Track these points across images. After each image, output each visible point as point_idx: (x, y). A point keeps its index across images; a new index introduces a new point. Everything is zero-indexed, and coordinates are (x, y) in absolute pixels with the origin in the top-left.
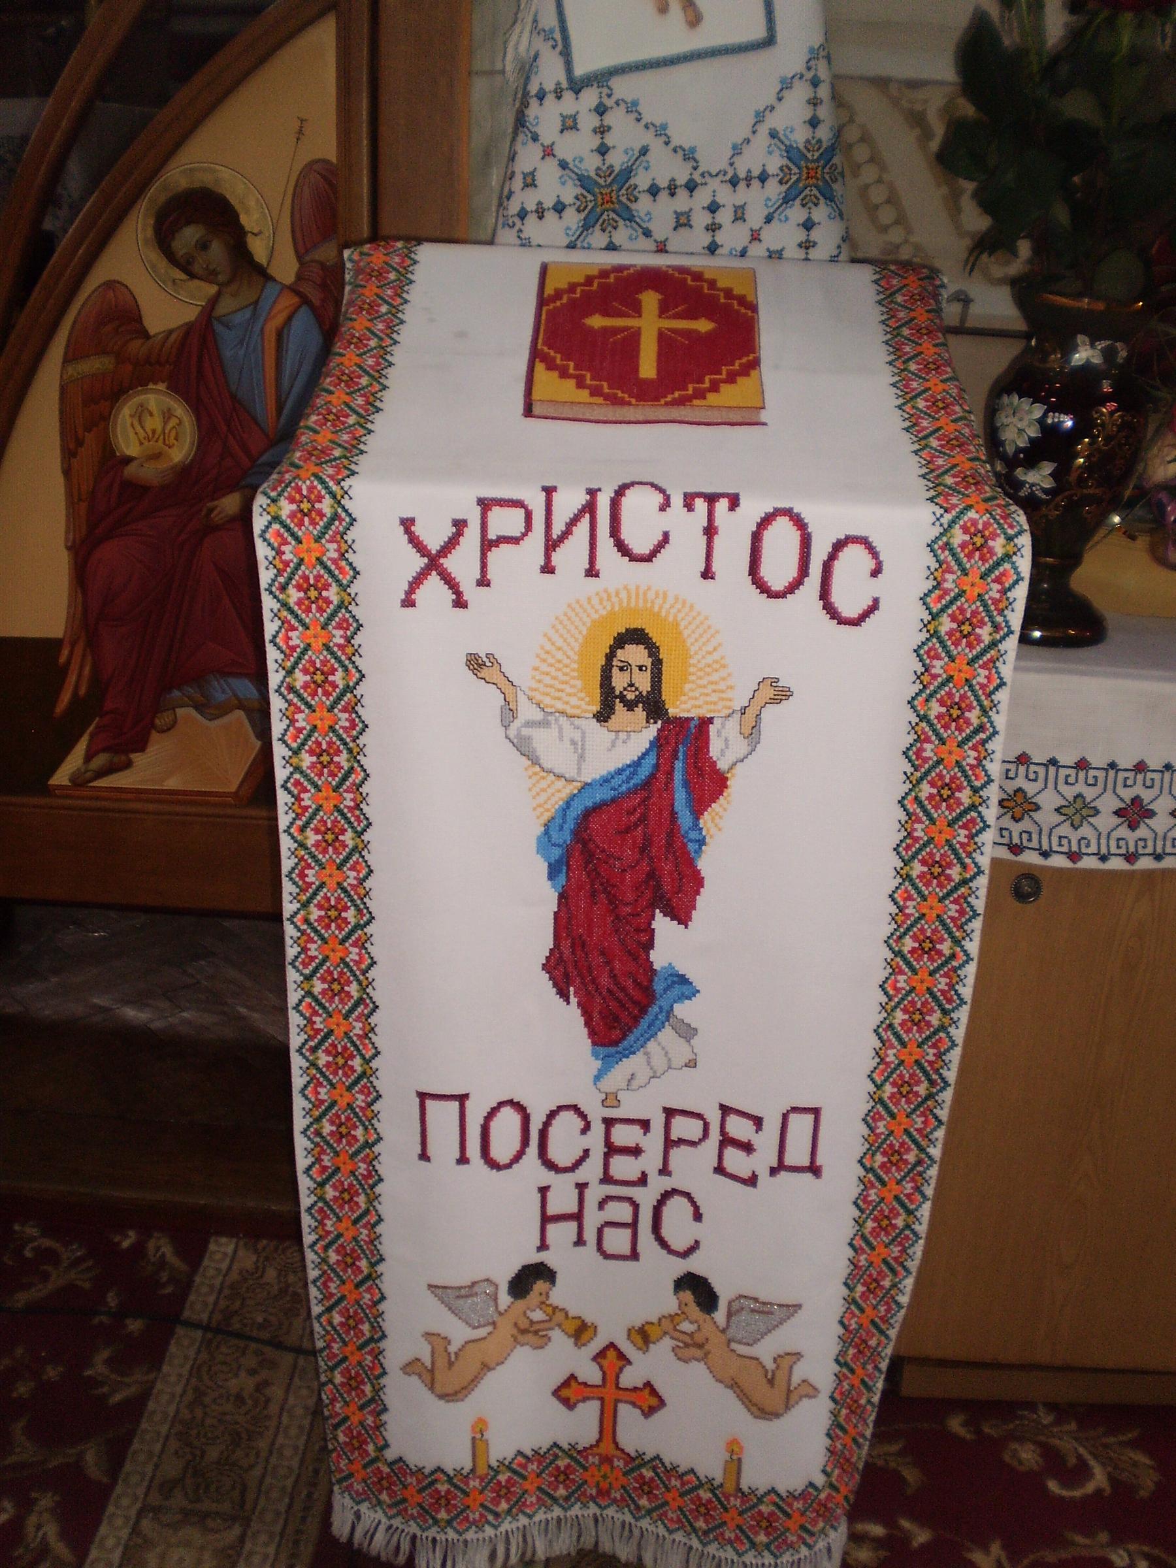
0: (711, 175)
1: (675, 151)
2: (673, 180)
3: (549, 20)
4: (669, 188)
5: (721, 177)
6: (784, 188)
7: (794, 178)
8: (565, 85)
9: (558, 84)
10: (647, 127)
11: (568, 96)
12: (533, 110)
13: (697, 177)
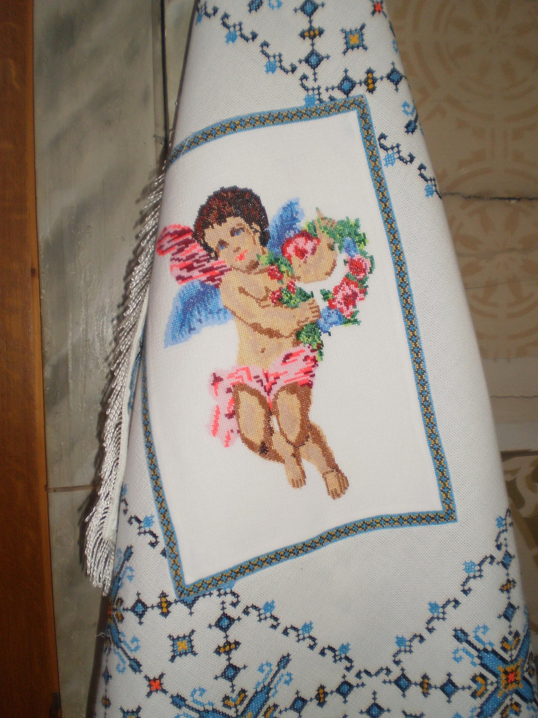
0: (368, 673)
1: (322, 653)
2: (322, 687)
3: (144, 505)
4: (318, 697)
5: (383, 676)
6: (479, 702)
7: (491, 688)
8: (172, 596)
9: (163, 595)
10: (285, 632)
11: (179, 610)
12: (129, 626)
13: (351, 678)
